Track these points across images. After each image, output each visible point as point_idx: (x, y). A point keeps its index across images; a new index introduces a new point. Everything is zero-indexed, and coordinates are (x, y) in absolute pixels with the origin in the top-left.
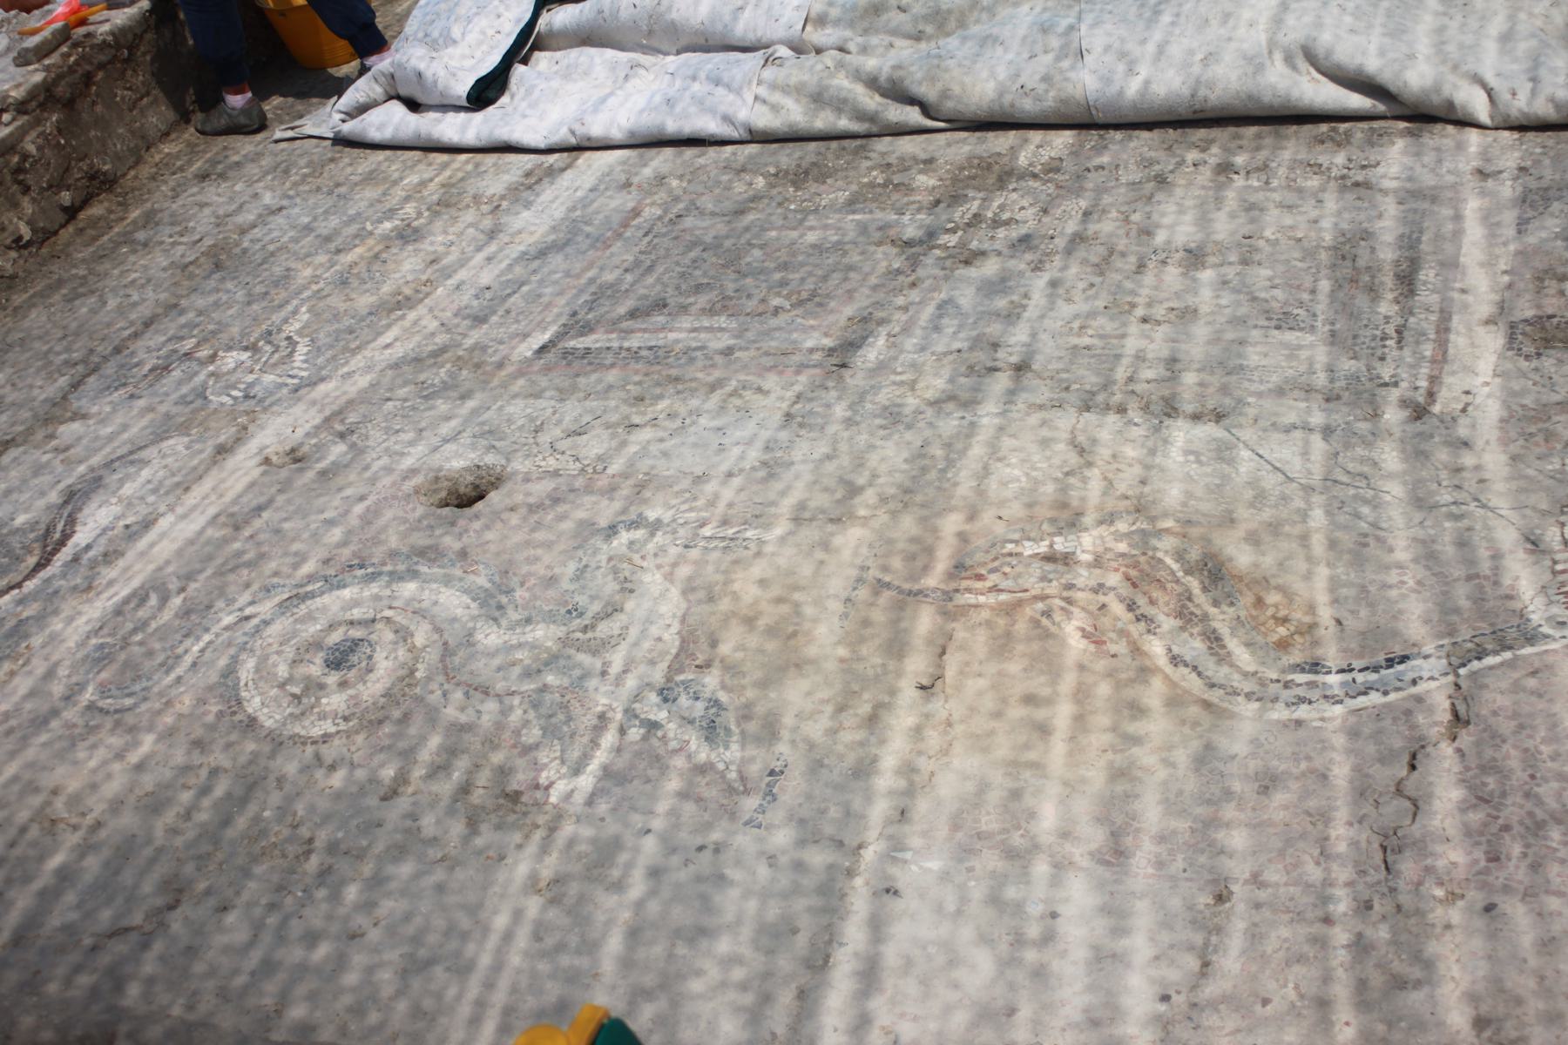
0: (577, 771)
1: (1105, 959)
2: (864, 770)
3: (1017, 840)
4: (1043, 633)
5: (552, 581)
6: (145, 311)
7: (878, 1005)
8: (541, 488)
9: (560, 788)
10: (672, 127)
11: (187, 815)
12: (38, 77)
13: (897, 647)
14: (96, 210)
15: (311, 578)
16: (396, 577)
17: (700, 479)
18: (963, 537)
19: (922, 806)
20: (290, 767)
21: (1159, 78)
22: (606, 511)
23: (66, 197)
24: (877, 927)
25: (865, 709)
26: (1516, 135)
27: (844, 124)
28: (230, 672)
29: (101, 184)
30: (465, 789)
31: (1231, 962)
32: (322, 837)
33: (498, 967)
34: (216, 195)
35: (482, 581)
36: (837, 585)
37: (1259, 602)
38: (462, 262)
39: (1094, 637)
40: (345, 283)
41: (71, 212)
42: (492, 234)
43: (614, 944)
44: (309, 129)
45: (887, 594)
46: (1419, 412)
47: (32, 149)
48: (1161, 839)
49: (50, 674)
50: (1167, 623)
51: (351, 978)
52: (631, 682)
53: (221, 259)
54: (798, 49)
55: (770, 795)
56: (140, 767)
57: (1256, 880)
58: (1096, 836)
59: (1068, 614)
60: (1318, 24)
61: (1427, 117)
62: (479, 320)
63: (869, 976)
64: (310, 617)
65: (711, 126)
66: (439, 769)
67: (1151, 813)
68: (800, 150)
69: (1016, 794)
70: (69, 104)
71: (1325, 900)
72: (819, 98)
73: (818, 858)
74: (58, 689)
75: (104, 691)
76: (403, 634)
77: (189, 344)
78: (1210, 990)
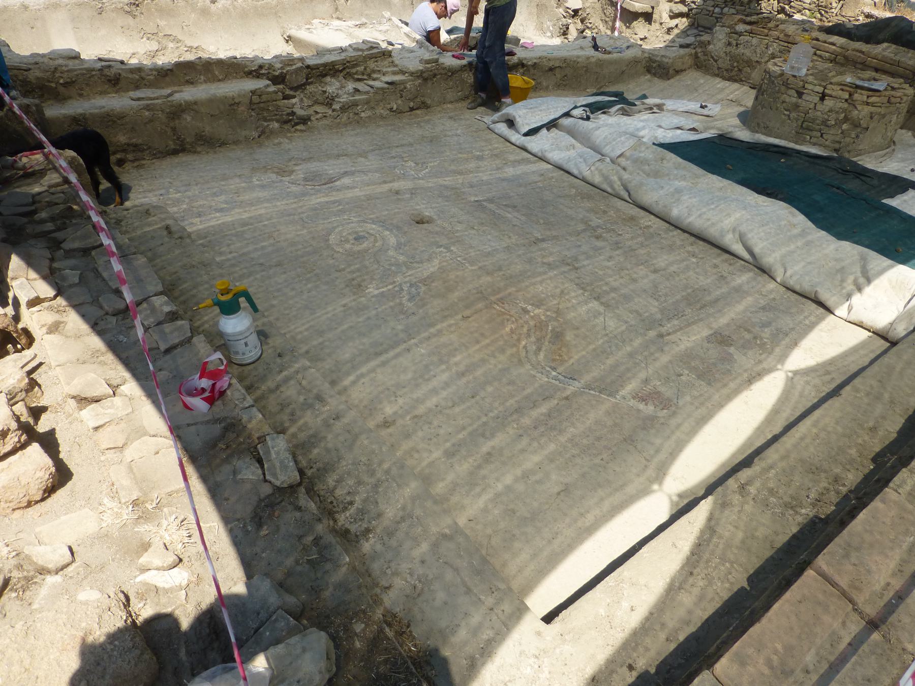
0: (377, 289)
1: (434, 391)
2: (432, 325)
3: (445, 359)
4: (502, 325)
5: (416, 249)
6: (404, 142)
7: (379, 371)
8: (438, 229)
9: (371, 290)
10: (566, 167)
11: (297, 251)
12: (421, 68)
13: (467, 307)
14: (418, 112)
15: (371, 219)
16: (387, 229)
17: (471, 247)
18: (510, 294)
19: (434, 340)
20: (325, 253)
21: (695, 221)
22: (445, 241)
23: (412, 104)
24: (397, 356)
25: (446, 314)
26: (784, 289)
27: (609, 190)
28: (334, 228)
29: (425, 106)
30: (353, 280)
31: (457, 410)
32: (317, 271)
33: (319, 317)
34: (449, 124)
35: (403, 240)
36: (471, 286)
37: (560, 349)
38: (483, 172)
39: (512, 331)
40: (453, 161)
41: (412, 109)
42: (498, 169)
43: (345, 327)
44: (485, 120)
45: (480, 295)
46: (661, 336)
47: (408, 87)
48: (475, 378)
49: (301, 207)
50: (533, 339)
51: (291, 302)
52: (407, 279)
53: (432, 140)
54: (613, 161)
55: (408, 317)
56: (298, 235)
57: (483, 399)
58: (462, 368)
59: (513, 322)
60: (752, 230)
61: (764, 271)
62: (472, 187)
63: (384, 364)
64: (362, 227)
65: (575, 172)
66: (353, 272)
67: (479, 372)
68: (596, 191)
69: (456, 350)
70: (425, 80)
71: (491, 411)
72: (606, 178)
73: (402, 335)
74: (300, 210)
75: (307, 217)
76: (376, 241)
77: (405, 155)
78: (448, 411)
